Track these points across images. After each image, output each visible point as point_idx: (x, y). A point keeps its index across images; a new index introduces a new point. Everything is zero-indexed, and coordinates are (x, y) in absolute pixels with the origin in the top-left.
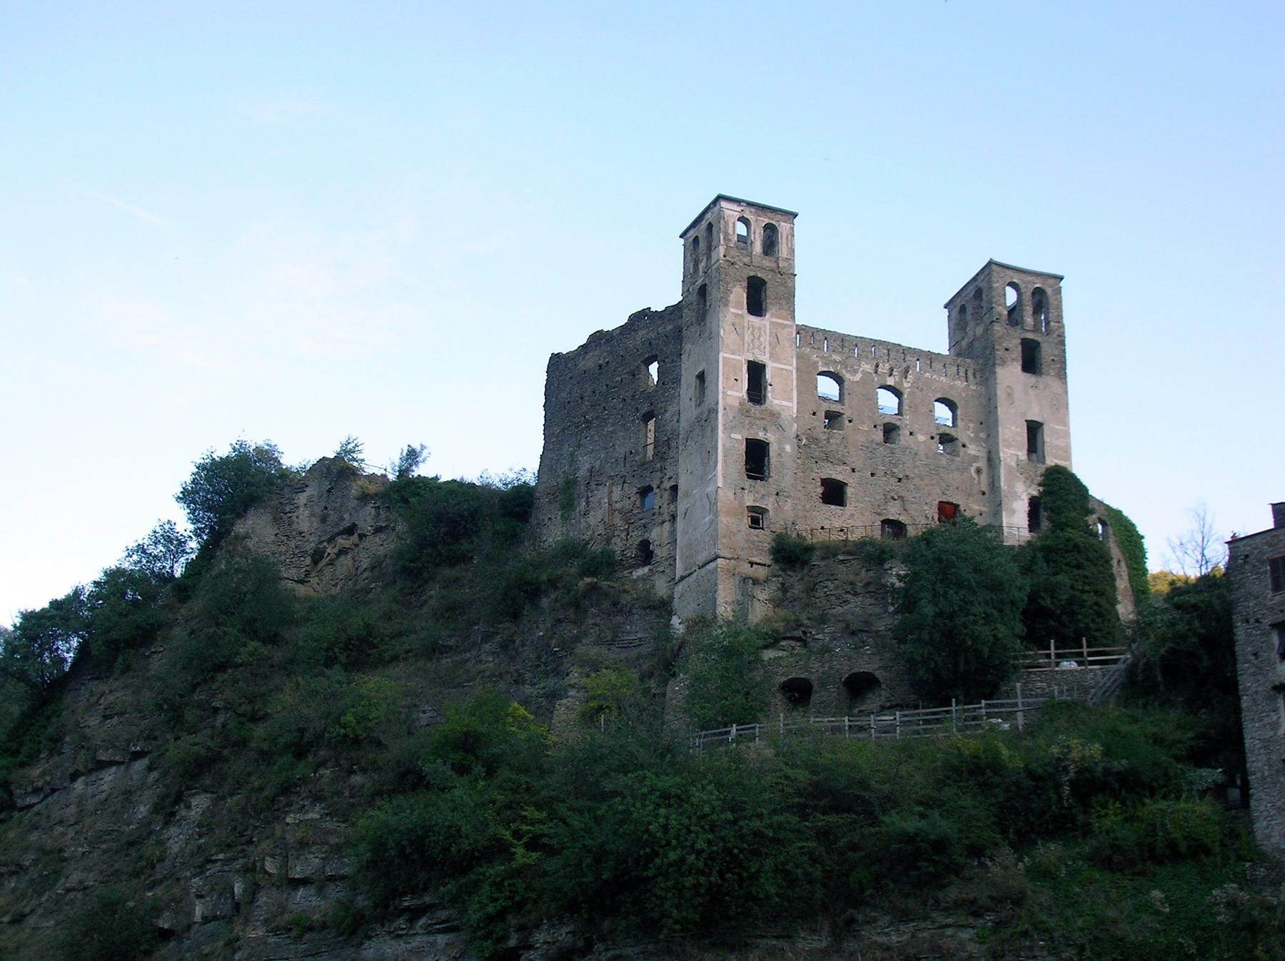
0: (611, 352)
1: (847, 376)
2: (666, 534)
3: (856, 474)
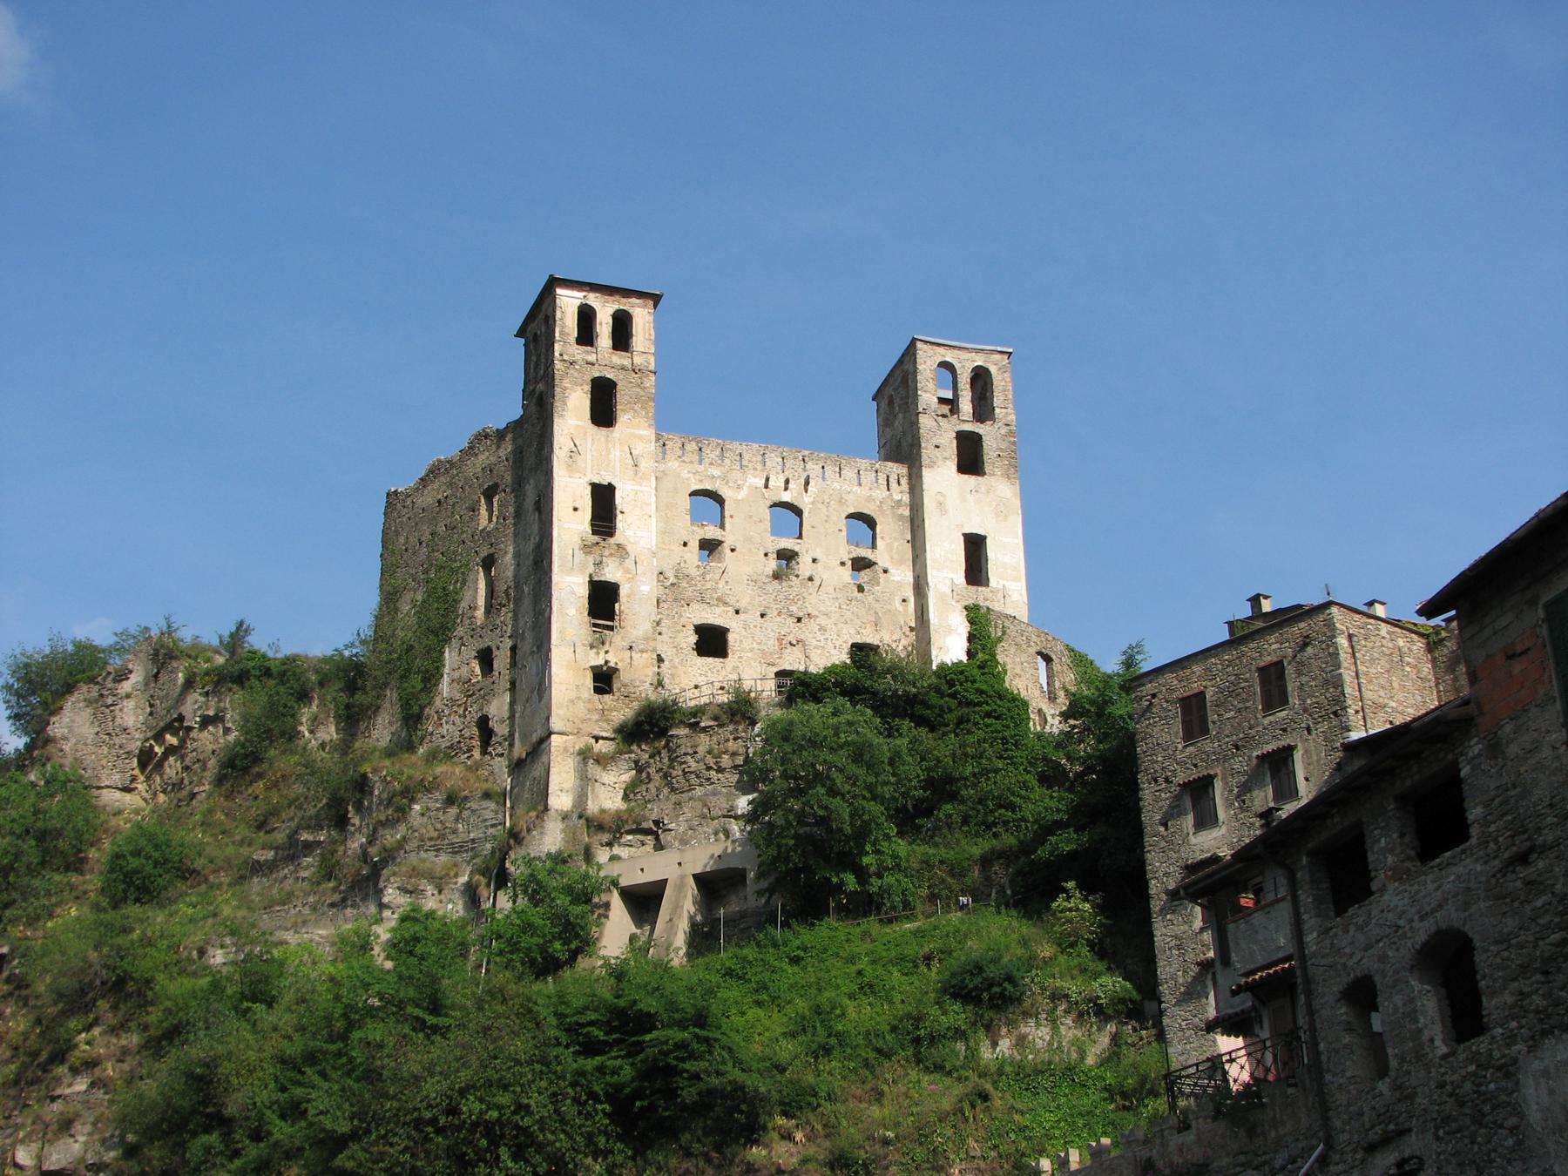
0: (451, 485)
1: (725, 492)
2: (507, 707)
3: (742, 616)
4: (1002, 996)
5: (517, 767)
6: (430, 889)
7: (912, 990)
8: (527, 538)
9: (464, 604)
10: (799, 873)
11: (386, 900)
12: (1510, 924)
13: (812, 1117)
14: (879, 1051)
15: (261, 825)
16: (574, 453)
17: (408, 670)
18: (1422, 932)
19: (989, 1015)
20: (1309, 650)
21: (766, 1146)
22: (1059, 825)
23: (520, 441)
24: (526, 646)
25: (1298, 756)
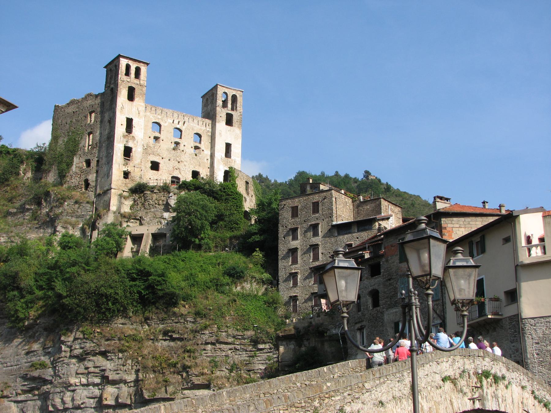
1: (162, 123)
3: (164, 160)
4: (240, 276)
5: (98, 196)
6: (70, 228)
7: (214, 272)
8: (105, 130)
9: (81, 145)
10: (181, 237)
11: (58, 229)
12: (386, 290)
13: (190, 302)
14: (207, 287)
15: (10, 200)
16: (122, 108)
17: (62, 161)
18: (371, 289)
19: (235, 280)
20: (326, 200)
21: (178, 308)
22: (255, 234)
23: (103, 100)
24: (104, 161)
25: (320, 226)
